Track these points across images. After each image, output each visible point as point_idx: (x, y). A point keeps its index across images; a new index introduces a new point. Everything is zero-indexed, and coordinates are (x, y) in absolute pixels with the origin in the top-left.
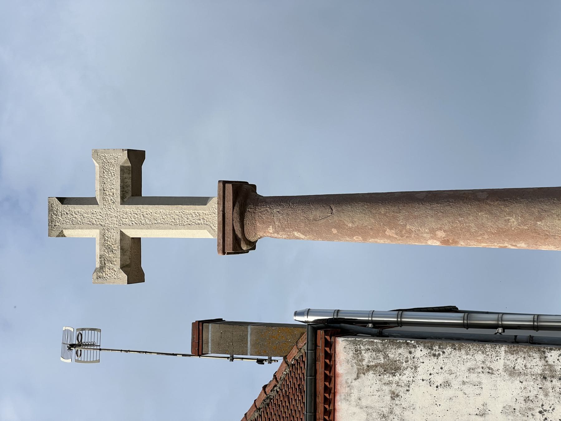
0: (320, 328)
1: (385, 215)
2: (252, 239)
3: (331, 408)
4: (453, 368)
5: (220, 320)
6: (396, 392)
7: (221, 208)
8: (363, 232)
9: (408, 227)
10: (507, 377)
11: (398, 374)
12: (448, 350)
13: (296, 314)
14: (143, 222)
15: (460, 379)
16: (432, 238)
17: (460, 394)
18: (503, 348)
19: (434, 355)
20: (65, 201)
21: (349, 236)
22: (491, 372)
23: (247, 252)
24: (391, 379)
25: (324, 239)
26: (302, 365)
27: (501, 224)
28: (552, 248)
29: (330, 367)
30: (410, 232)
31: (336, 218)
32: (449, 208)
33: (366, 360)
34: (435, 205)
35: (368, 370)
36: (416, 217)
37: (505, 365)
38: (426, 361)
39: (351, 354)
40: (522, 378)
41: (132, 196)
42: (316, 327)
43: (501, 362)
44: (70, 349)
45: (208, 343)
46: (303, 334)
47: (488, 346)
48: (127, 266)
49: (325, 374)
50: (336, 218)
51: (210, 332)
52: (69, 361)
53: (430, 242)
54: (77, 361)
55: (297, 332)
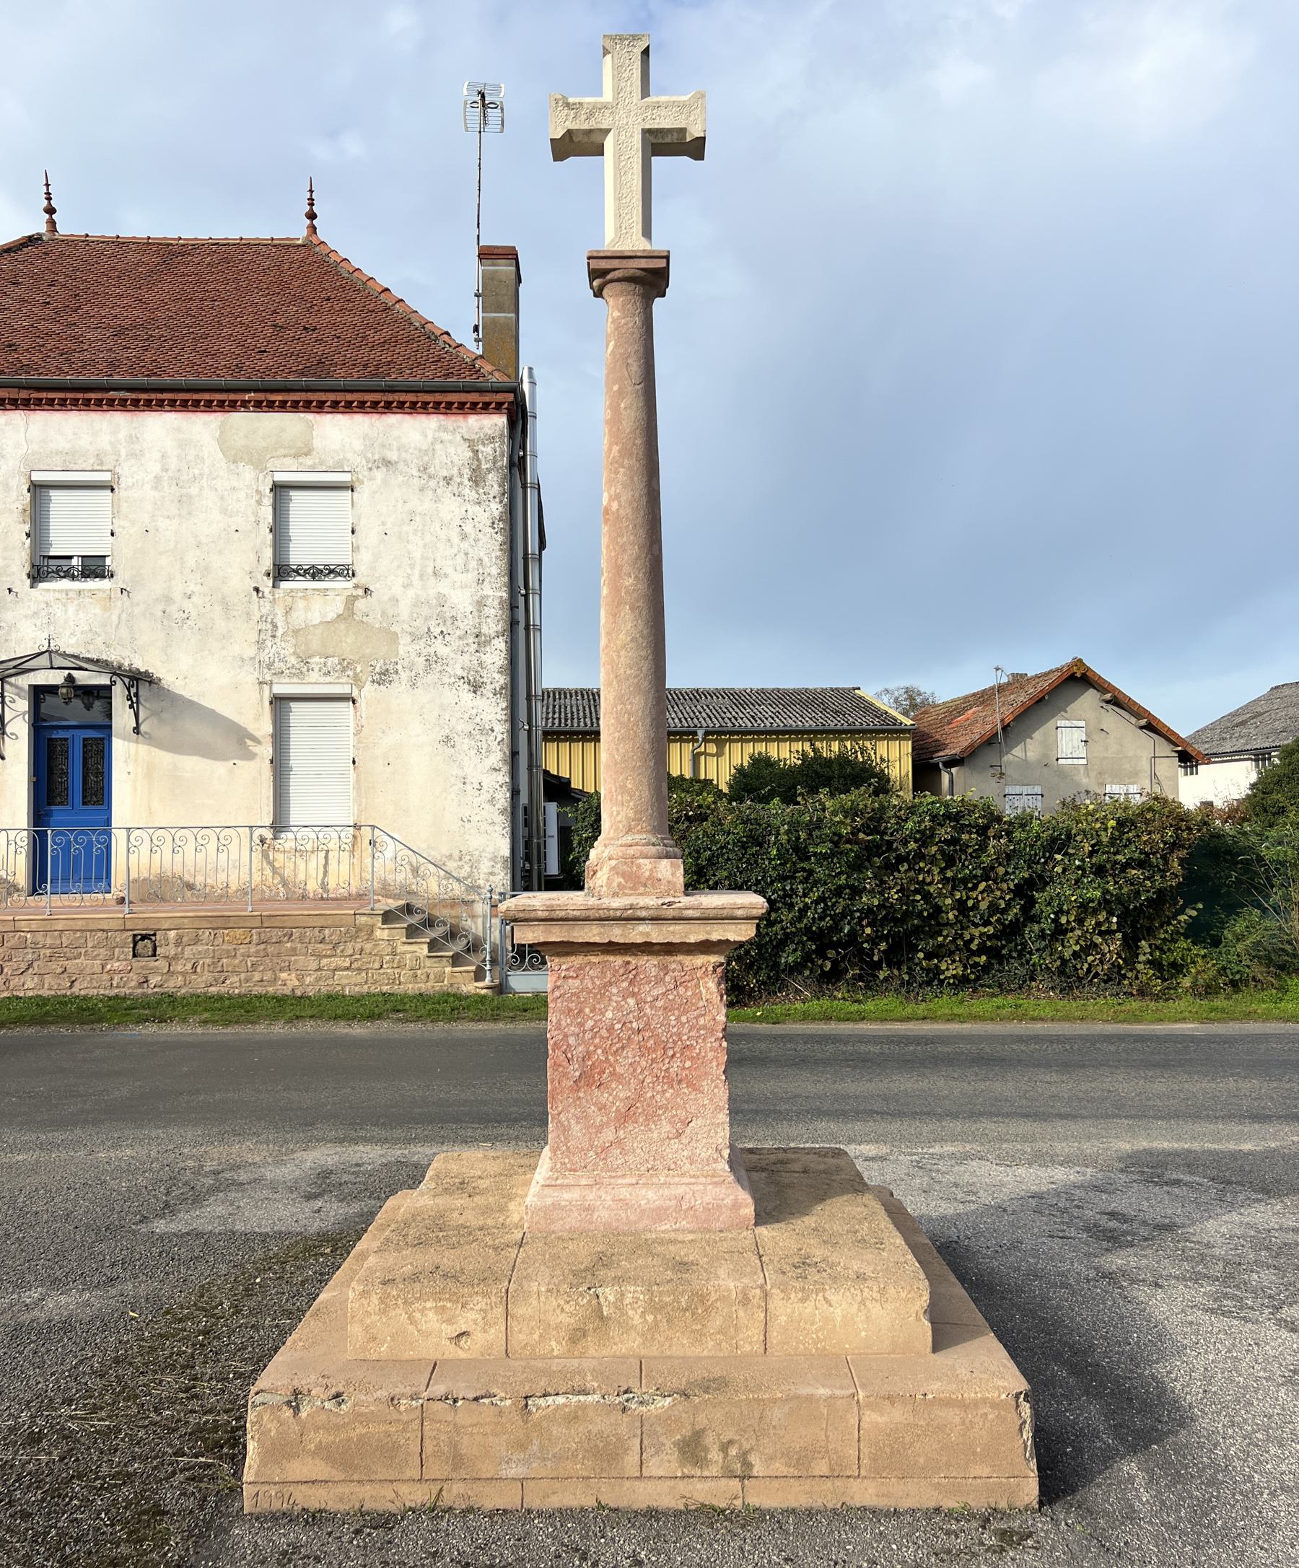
0: (515, 397)
1: (634, 444)
2: (605, 292)
3: (430, 410)
4: (480, 543)
5: (519, 280)
6: (452, 482)
7: (639, 254)
8: (615, 420)
9: (622, 470)
10: (476, 598)
11: (471, 483)
12: (500, 538)
13: (530, 369)
14: (622, 158)
15: (470, 551)
16: (610, 496)
17: (455, 550)
18: (505, 595)
19: (493, 523)
20: (645, 57)
21: (611, 404)
22: (480, 582)
23: (592, 287)
24: (466, 476)
25: (607, 376)
26: (474, 377)
27: (626, 569)
28: (603, 621)
29: (474, 408)
30: (617, 473)
31: (630, 388)
32: (642, 513)
33: (484, 449)
34: (645, 499)
35: (473, 451)
36: (632, 479)
37: (488, 596)
38: (487, 515)
39: (490, 432)
40: (476, 614)
41: (652, 144)
42: (516, 390)
43: (490, 593)
44: (479, 93)
45: (493, 265)
46: (509, 377)
47: (506, 579)
48: (571, 138)
49: (466, 403)
50: (630, 388)
51: (505, 268)
52: (465, 93)
53: (606, 495)
54: (466, 102)
55: (511, 371)
